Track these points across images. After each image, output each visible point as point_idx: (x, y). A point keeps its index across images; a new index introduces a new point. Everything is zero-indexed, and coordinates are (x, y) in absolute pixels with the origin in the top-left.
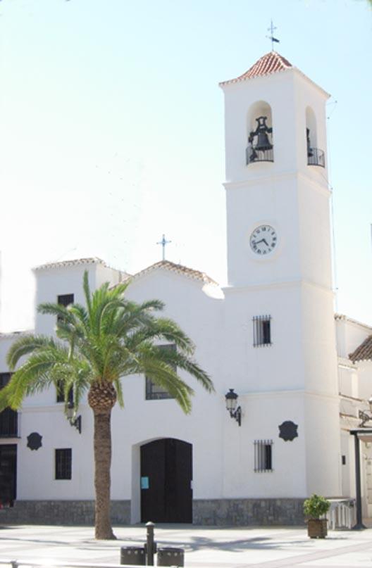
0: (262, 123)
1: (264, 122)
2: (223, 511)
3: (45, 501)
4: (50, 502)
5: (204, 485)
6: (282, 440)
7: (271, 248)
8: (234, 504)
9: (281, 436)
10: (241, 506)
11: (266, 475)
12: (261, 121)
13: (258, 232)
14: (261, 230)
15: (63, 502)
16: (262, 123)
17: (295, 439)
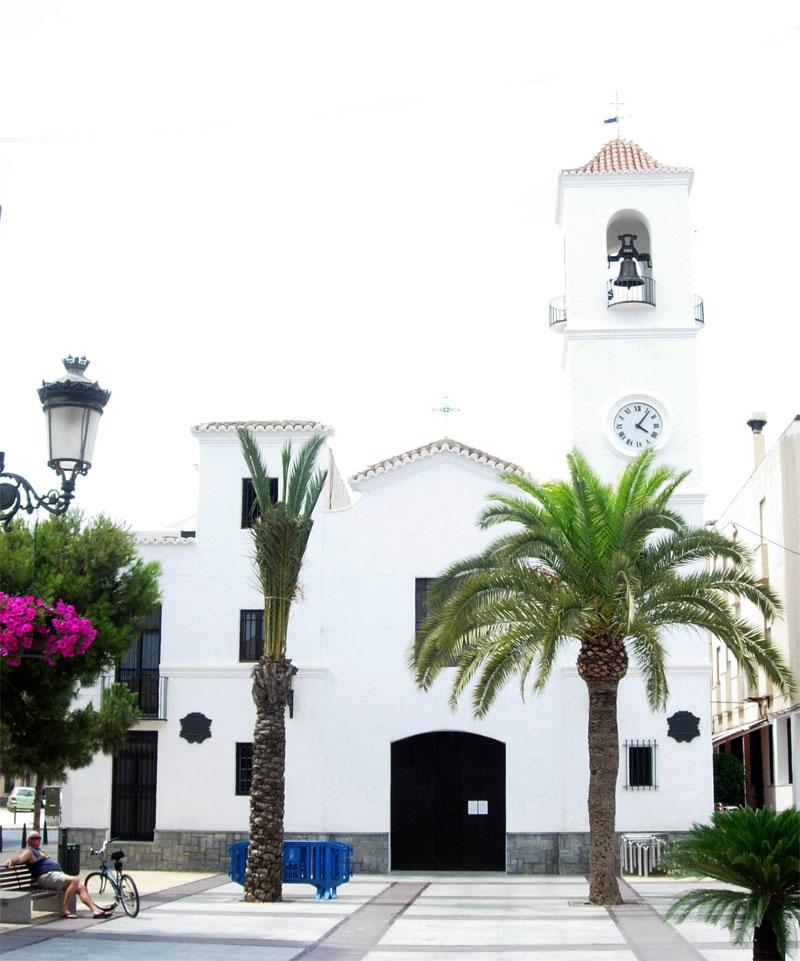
0: (628, 243)
1: (632, 242)
6: (672, 740)
9: (183, 734)
12: (628, 241)
16: (628, 243)
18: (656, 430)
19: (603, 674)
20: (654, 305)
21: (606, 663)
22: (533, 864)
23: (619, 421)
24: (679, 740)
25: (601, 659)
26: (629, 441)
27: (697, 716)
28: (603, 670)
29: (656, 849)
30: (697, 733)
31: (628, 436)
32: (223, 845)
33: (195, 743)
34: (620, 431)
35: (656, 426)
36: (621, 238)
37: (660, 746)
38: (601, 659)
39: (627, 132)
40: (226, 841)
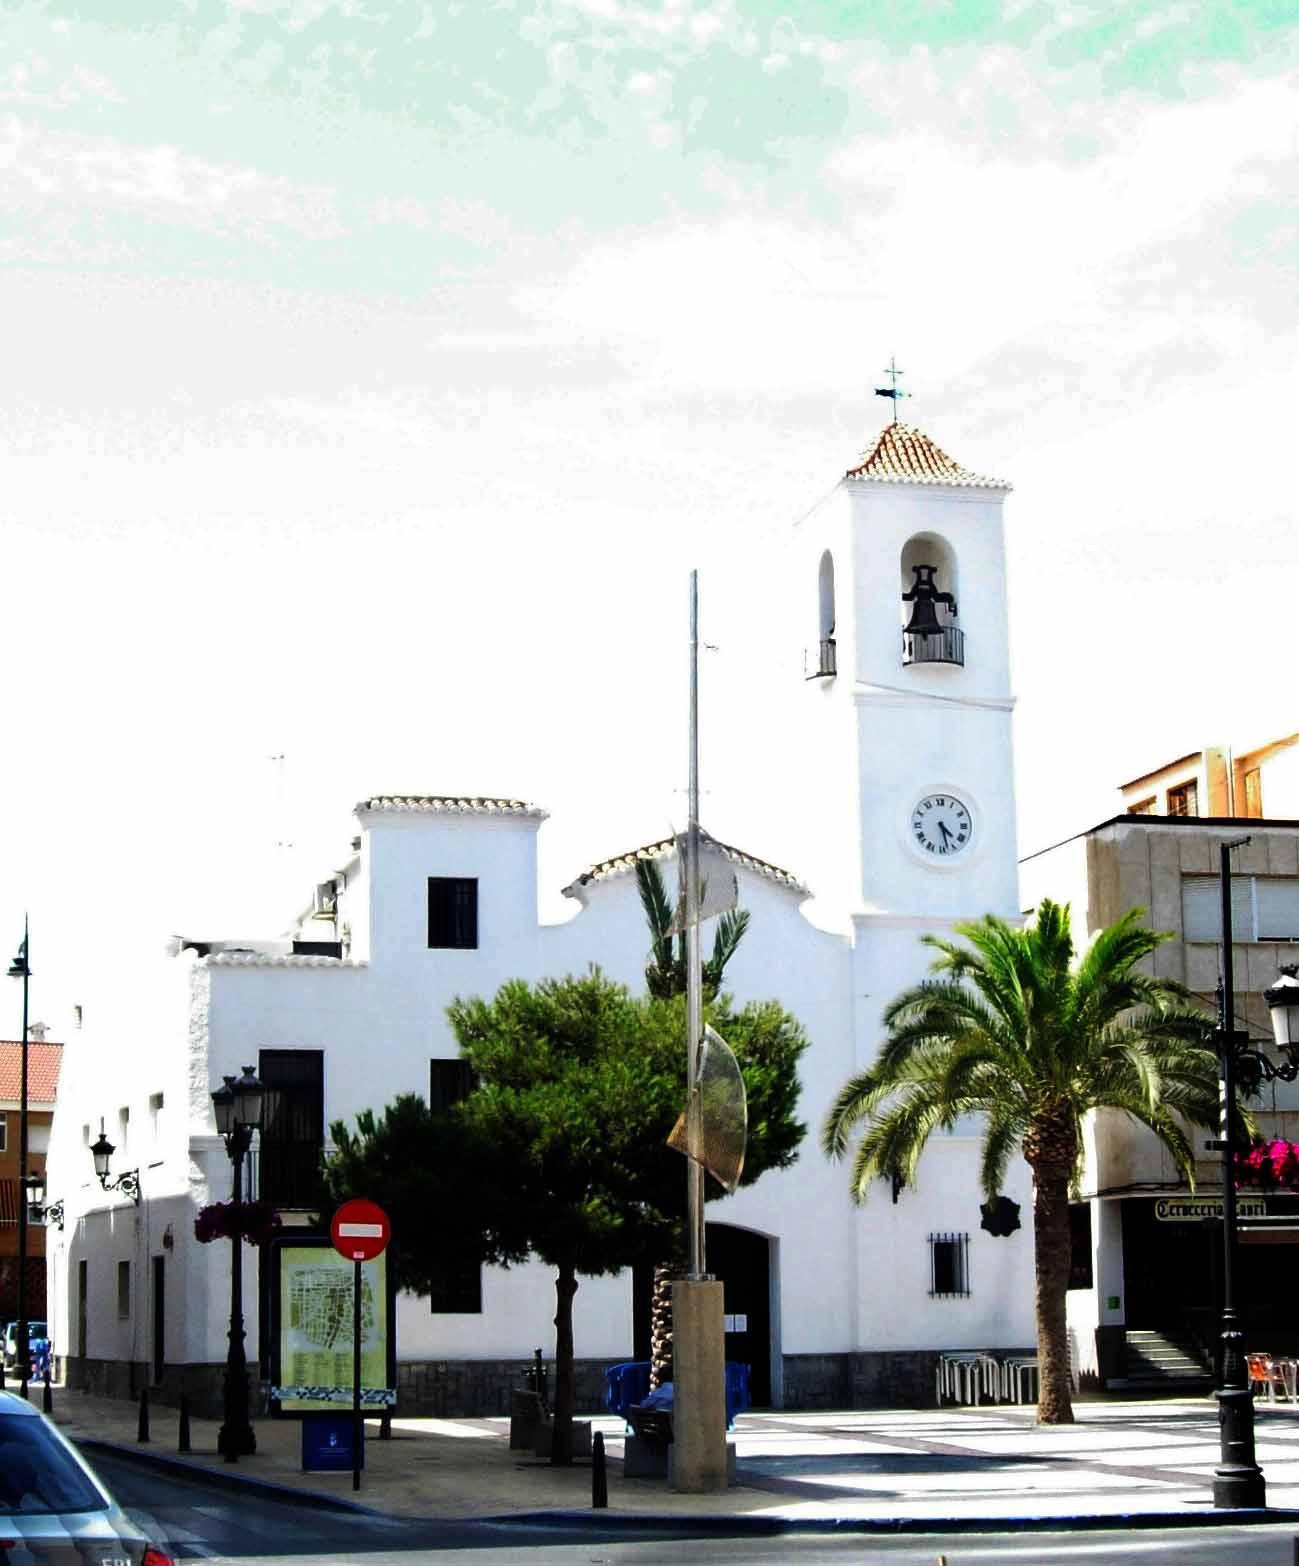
0: (925, 577)
1: (930, 576)
2: (866, 1378)
3: (417, 1363)
4: (433, 1365)
5: (804, 1326)
6: (987, 1234)
7: (957, 843)
8: (894, 1363)
9: (984, 1225)
10: (908, 1366)
11: (950, 1303)
12: (925, 573)
13: (928, 806)
14: (934, 803)
15: (472, 1364)
16: (925, 577)
17: (1015, 1233)
18: (963, 832)
19: (1060, 1157)
20: (962, 664)
21: (1063, 1146)
22: (815, 1395)
23: (918, 819)
24: (995, 1234)
25: (1059, 1140)
26: (930, 844)
27: (1017, 1203)
28: (1060, 1154)
29: (987, 1367)
30: (1017, 1225)
31: (929, 838)
32: (423, 1380)
33: (1001, 1237)
34: (919, 831)
35: (964, 826)
36: (917, 570)
37: (973, 1241)
38: (1059, 1140)
39: (913, 417)
40: (426, 1375)
